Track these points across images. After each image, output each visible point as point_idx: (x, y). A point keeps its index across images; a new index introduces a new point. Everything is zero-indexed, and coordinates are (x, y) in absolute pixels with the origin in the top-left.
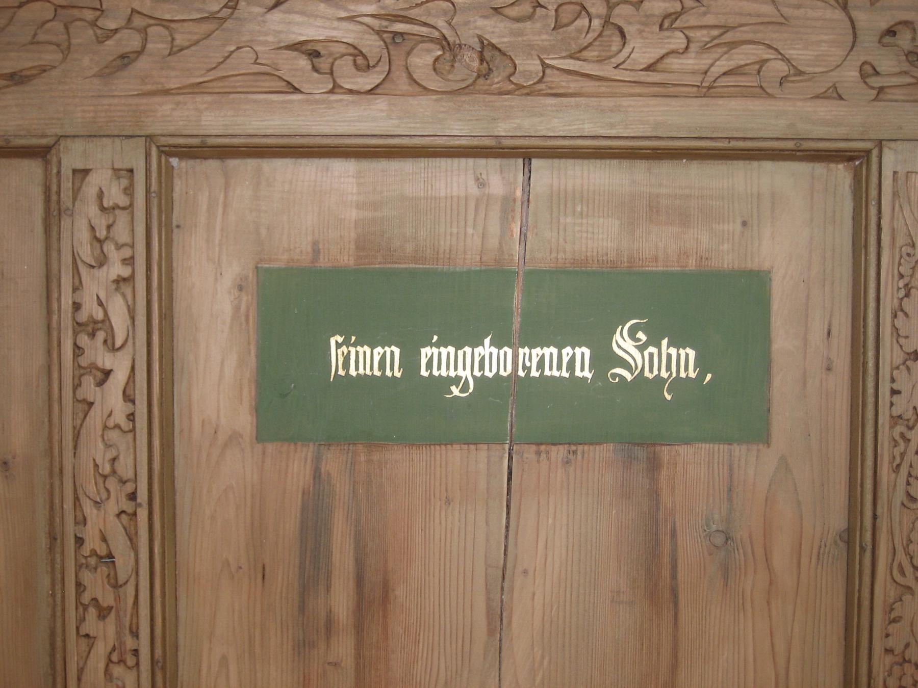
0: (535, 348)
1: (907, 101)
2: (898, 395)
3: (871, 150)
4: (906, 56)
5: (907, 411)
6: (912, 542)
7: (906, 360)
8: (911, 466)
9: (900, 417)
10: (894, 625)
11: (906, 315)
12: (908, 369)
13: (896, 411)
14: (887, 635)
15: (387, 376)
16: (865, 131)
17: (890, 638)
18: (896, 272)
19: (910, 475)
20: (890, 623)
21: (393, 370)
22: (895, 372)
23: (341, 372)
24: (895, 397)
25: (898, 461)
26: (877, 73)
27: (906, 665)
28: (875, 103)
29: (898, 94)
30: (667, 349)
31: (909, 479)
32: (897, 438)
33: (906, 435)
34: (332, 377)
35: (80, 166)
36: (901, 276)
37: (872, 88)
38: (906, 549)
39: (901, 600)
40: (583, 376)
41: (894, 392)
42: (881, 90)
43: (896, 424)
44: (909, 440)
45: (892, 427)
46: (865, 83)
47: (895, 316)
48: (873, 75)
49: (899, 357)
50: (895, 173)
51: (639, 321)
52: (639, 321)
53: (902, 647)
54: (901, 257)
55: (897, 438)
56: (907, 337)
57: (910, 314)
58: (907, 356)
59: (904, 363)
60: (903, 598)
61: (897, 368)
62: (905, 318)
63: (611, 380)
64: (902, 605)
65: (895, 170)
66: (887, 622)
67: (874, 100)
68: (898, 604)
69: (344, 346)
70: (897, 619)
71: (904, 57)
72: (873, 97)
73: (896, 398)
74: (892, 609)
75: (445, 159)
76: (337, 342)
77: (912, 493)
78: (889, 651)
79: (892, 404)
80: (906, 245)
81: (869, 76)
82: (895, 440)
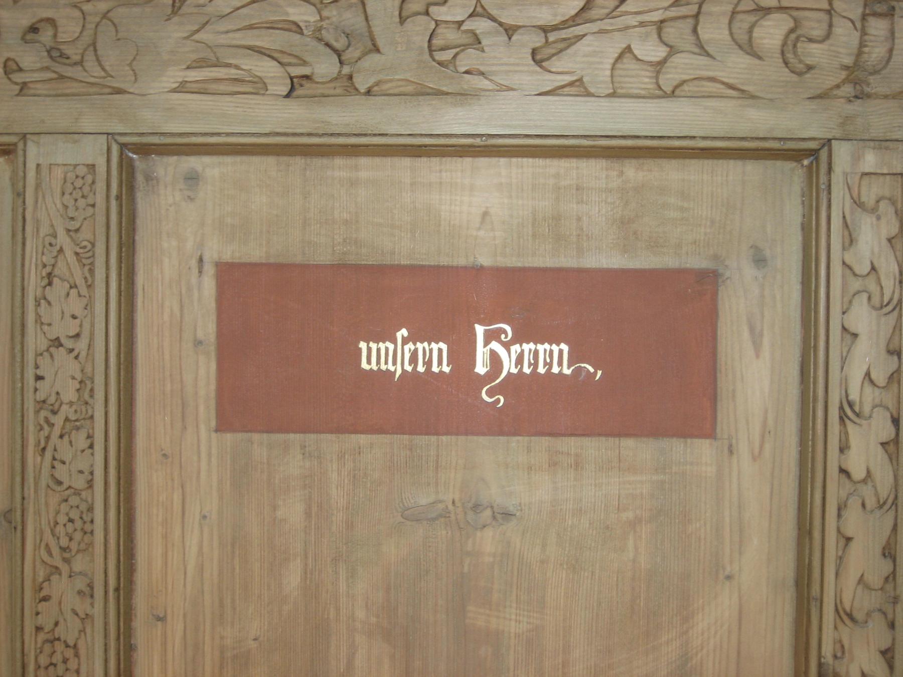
1: (49, 96)
2: (42, 381)
3: (828, 143)
4: (48, 52)
5: (50, 396)
6: (58, 523)
7: (50, 346)
8: (55, 450)
9: (44, 402)
10: (43, 603)
11: (49, 303)
12: (52, 356)
13: (41, 396)
14: (37, 614)
16: (9, 125)
17: (40, 616)
18: (39, 262)
19: (54, 459)
20: (40, 601)
21: (441, 365)
22: (39, 358)
23: (409, 368)
24: (38, 382)
25: (43, 444)
26: (20, 70)
27: (57, 643)
28: (19, 98)
29: (41, 88)
31: (54, 462)
32: (42, 422)
33: (49, 419)
36: (45, 266)
37: (16, 84)
39: (49, 580)
40: (387, 369)
41: (39, 378)
42: (24, 85)
43: (41, 409)
44: (53, 425)
45: (37, 412)
46: (9, 79)
47: (38, 305)
48: (17, 71)
49: (43, 344)
50: (38, 165)
53: (51, 626)
54: (44, 247)
55: (42, 422)
56: (49, 325)
57: (53, 303)
58: (51, 343)
59: (47, 350)
60: (52, 578)
61: (41, 354)
62: (47, 305)
64: (50, 584)
65: (38, 162)
66: (37, 601)
67: (18, 95)
68: (46, 584)
69: (411, 343)
70: (47, 598)
71: (46, 54)
72: (17, 92)
73: (40, 384)
74: (41, 589)
77: (57, 476)
78: (39, 629)
79: (36, 390)
80: (49, 235)
81: (14, 71)
82: (40, 425)
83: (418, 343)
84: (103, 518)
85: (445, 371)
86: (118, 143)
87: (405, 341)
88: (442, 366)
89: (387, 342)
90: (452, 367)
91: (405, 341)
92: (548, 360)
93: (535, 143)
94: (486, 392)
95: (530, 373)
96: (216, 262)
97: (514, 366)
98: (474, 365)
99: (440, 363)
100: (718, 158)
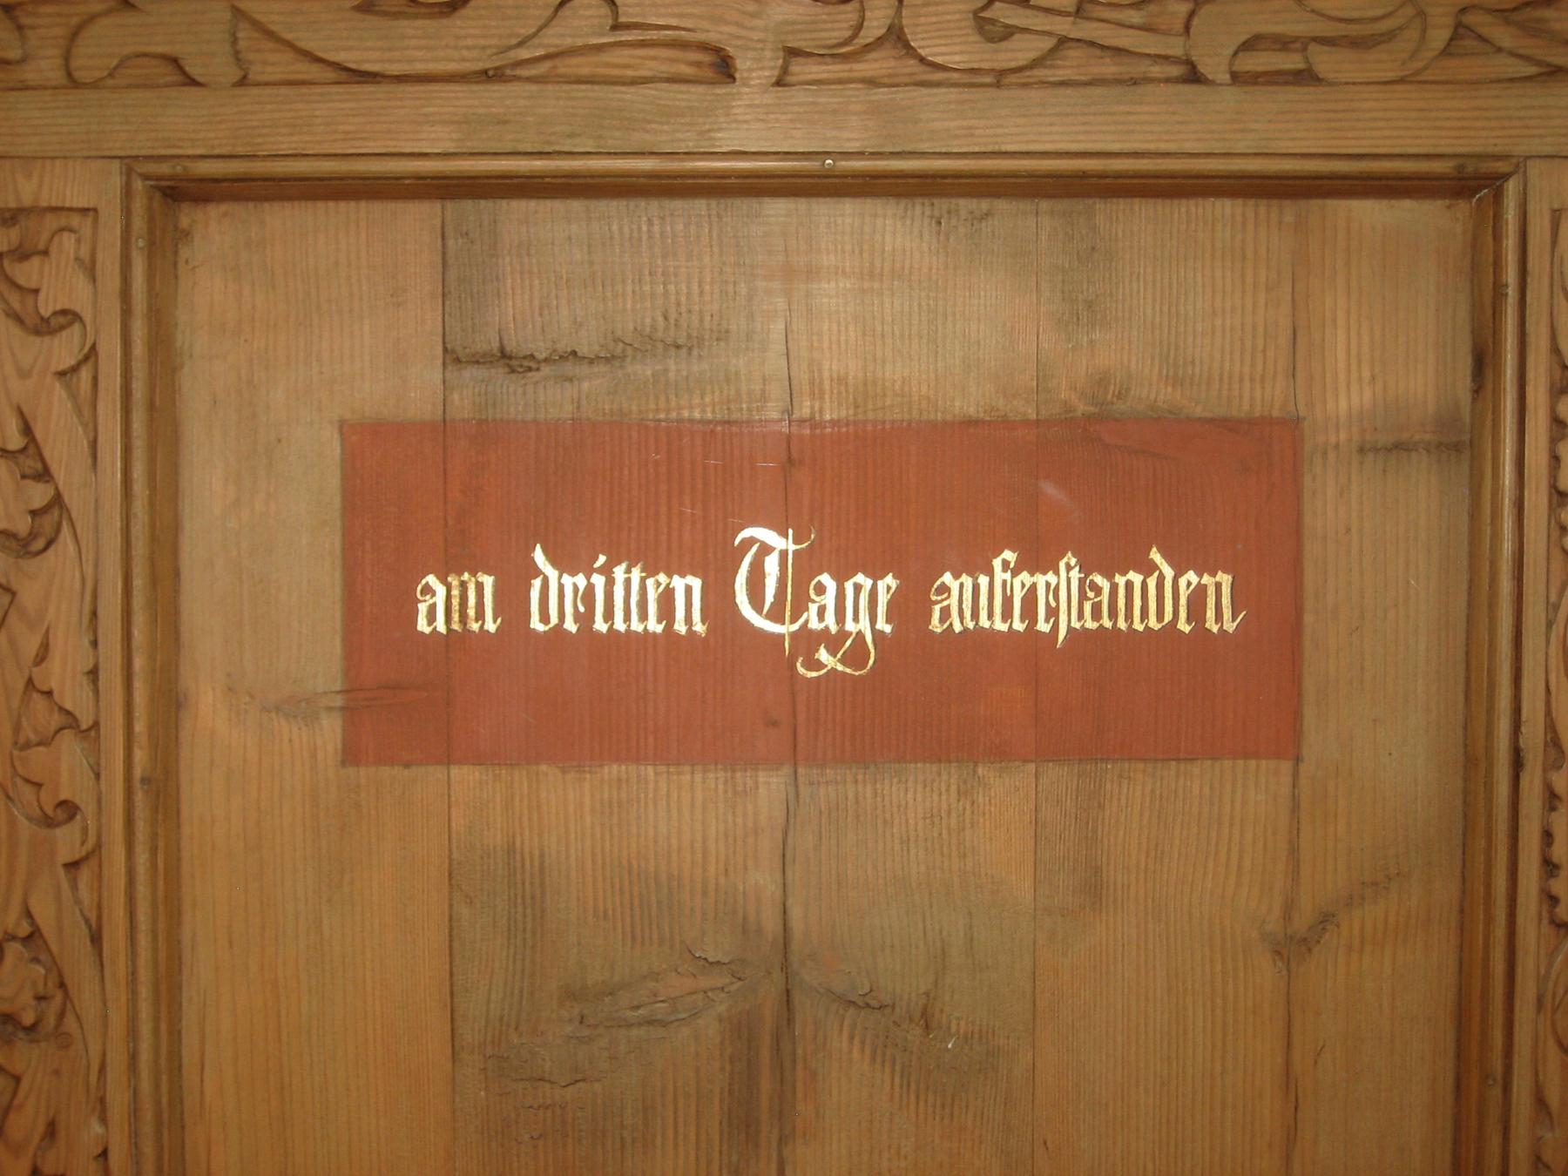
0: (882, 578)
15: (488, 631)
21: (630, 620)
23: (1076, 624)
30: (57, 489)
34: (1241, 616)
75: (1319, 202)
83: (676, 577)
84: (103, 869)
85: (569, 629)
88: (1148, 618)
89: (1131, 572)
90: (501, 623)
93: (1163, 167)
94: (807, 669)
95: (663, 631)
96: (1296, 423)
97: (817, 618)
100: (567, 198)
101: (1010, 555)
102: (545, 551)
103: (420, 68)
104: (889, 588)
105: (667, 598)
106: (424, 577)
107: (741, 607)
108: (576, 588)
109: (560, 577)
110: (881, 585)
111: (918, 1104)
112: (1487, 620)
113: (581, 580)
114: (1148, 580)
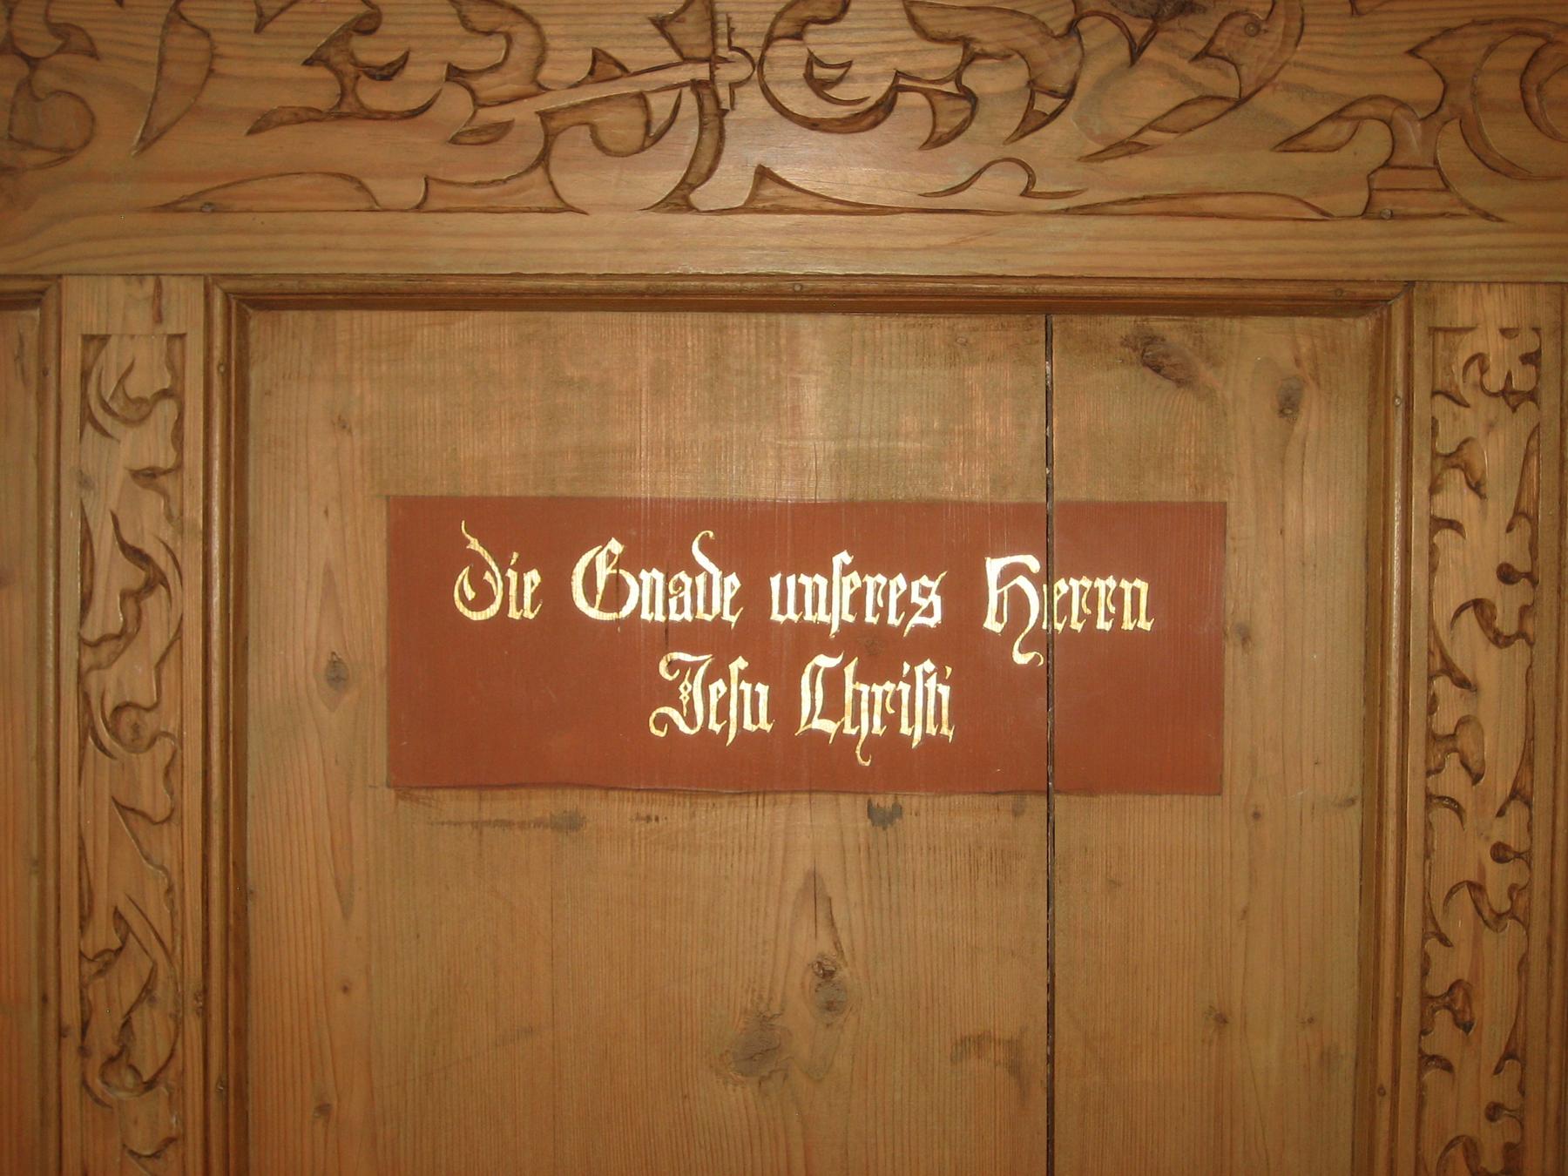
35: (174, 331)
38: (196, 204)
51: (1027, 631)
52: (1027, 631)
63: (858, 752)
76: (924, 672)
85: (750, 729)
86: (221, 289)
87: (846, 571)
89: (654, 570)
91: (846, 571)
92: (881, 604)
98: (770, 614)
99: (1135, 615)
101: (615, 547)
102: (482, 543)
103: (926, 216)
104: (733, 588)
105: (1118, 597)
106: (536, 616)
107: (803, 681)
108: (1108, 589)
109: (753, 687)
110: (893, 583)
111: (1526, 246)
112: (118, 599)
113: (889, 686)
114: (891, 582)
